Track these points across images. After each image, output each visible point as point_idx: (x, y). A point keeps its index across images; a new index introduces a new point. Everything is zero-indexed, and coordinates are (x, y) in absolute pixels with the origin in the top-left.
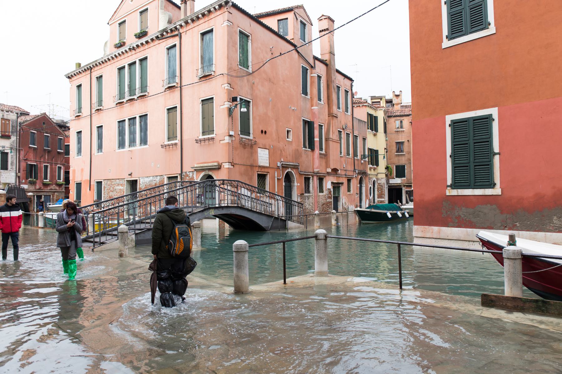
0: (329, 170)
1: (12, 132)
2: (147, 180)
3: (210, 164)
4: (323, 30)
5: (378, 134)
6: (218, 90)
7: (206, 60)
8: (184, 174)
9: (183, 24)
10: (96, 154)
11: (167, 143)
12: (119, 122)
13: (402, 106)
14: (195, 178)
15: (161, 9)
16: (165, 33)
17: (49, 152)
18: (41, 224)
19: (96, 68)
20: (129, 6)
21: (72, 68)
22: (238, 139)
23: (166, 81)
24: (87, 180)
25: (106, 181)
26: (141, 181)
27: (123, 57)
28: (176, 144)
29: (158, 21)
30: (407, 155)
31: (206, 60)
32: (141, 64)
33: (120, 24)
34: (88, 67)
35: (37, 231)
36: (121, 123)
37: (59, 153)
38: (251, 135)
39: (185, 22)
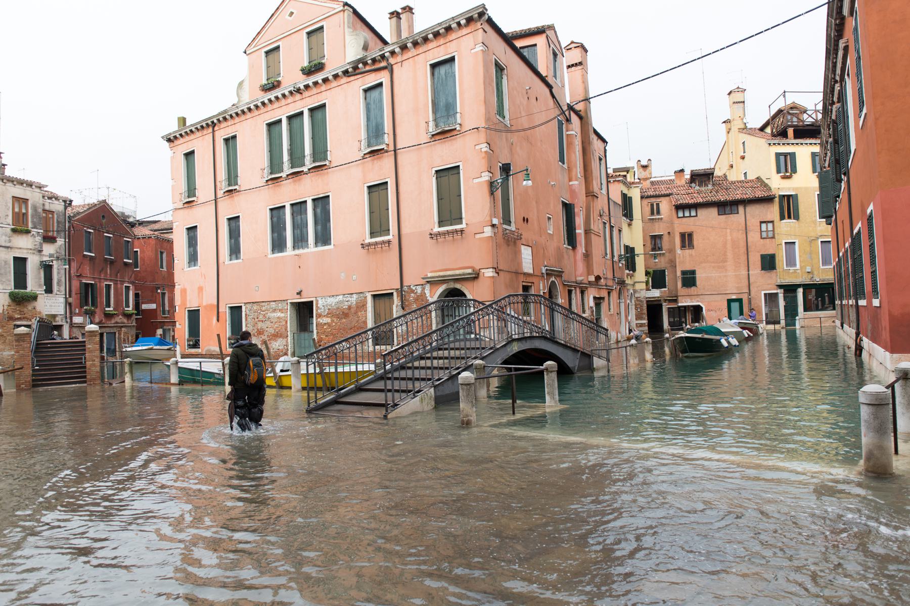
0: (592, 278)
1: (58, 231)
2: (332, 301)
3: (458, 272)
4: (573, 65)
5: (634, 222)
6: (470, 155)
7: (443, 107)
8: (405, 288)
9: (397, 50)
10: (227, 262)
11: (368, 240)
12: (271, 210)
13: (652, 183)
14: (428, 295)
15: (349, 27)
16: (360, 66)
17: (112, 262)
18: (174, 379)
19: (224, 124)
20: (283, 23)
21: (173, 127)
22: (500, 230)
23: (364, 143)
24: (212, 305)
25: (249, 306)
26: (320, 302)
27: (276, 105)
28: (389, 242)
29: (344, 47)
30: (667, 254)
31: (443, 107)
32: (312, 116)
33: (267, 53)
34: (209, 122)
35: (169, 391)
36: (275, 212)
37: (126, 264)
38: (513, 224)
39: (400, 47)
